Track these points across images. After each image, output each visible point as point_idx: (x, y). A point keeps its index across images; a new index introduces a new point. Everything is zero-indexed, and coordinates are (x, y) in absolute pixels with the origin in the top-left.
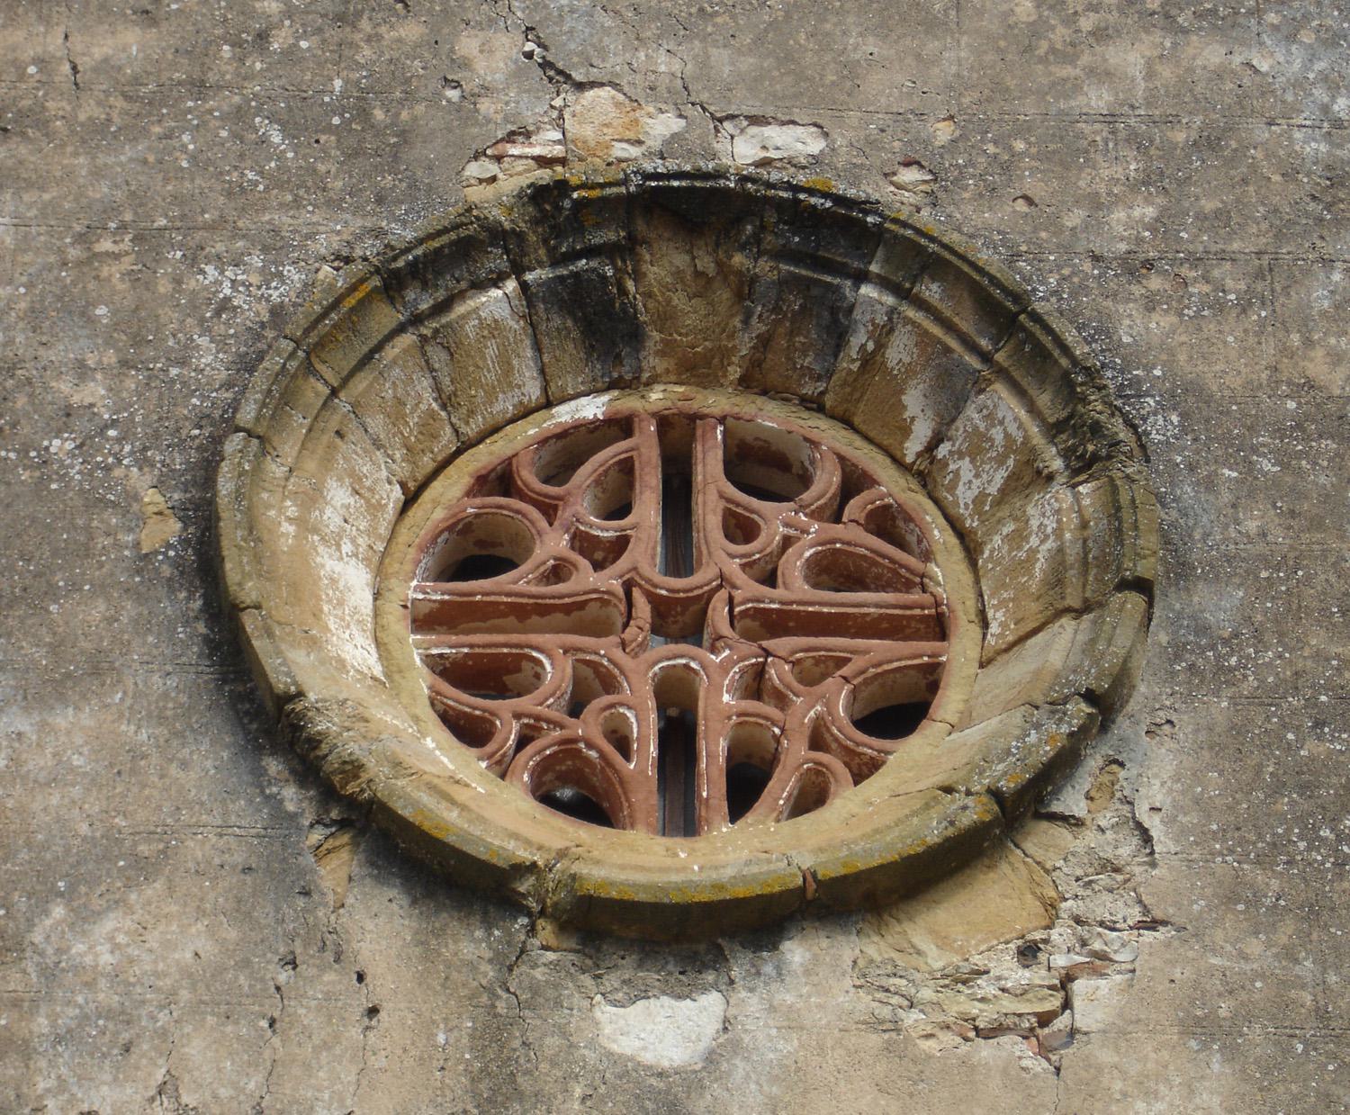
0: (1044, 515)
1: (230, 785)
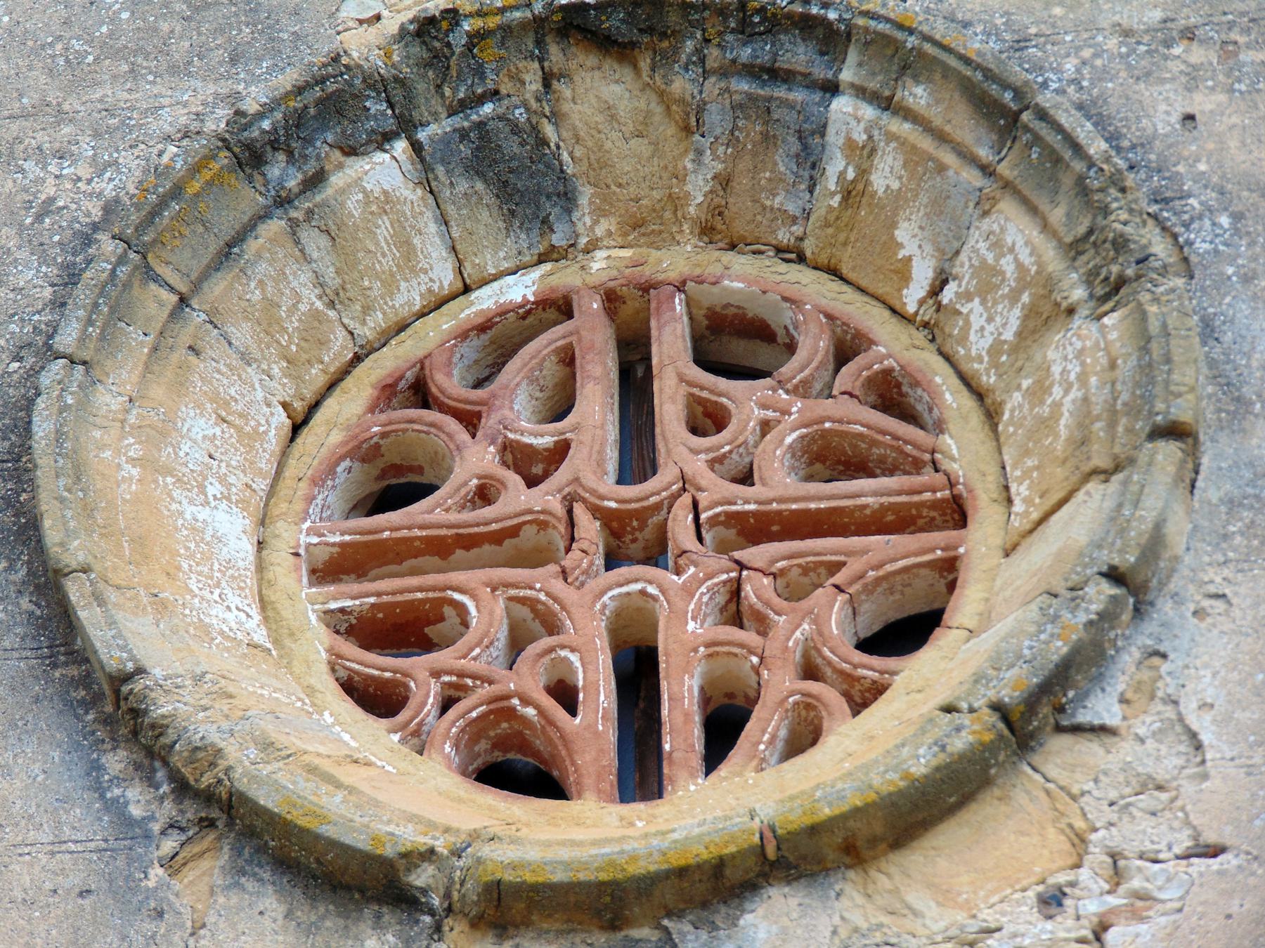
0: (1065, 358)
1: (62, 791)
